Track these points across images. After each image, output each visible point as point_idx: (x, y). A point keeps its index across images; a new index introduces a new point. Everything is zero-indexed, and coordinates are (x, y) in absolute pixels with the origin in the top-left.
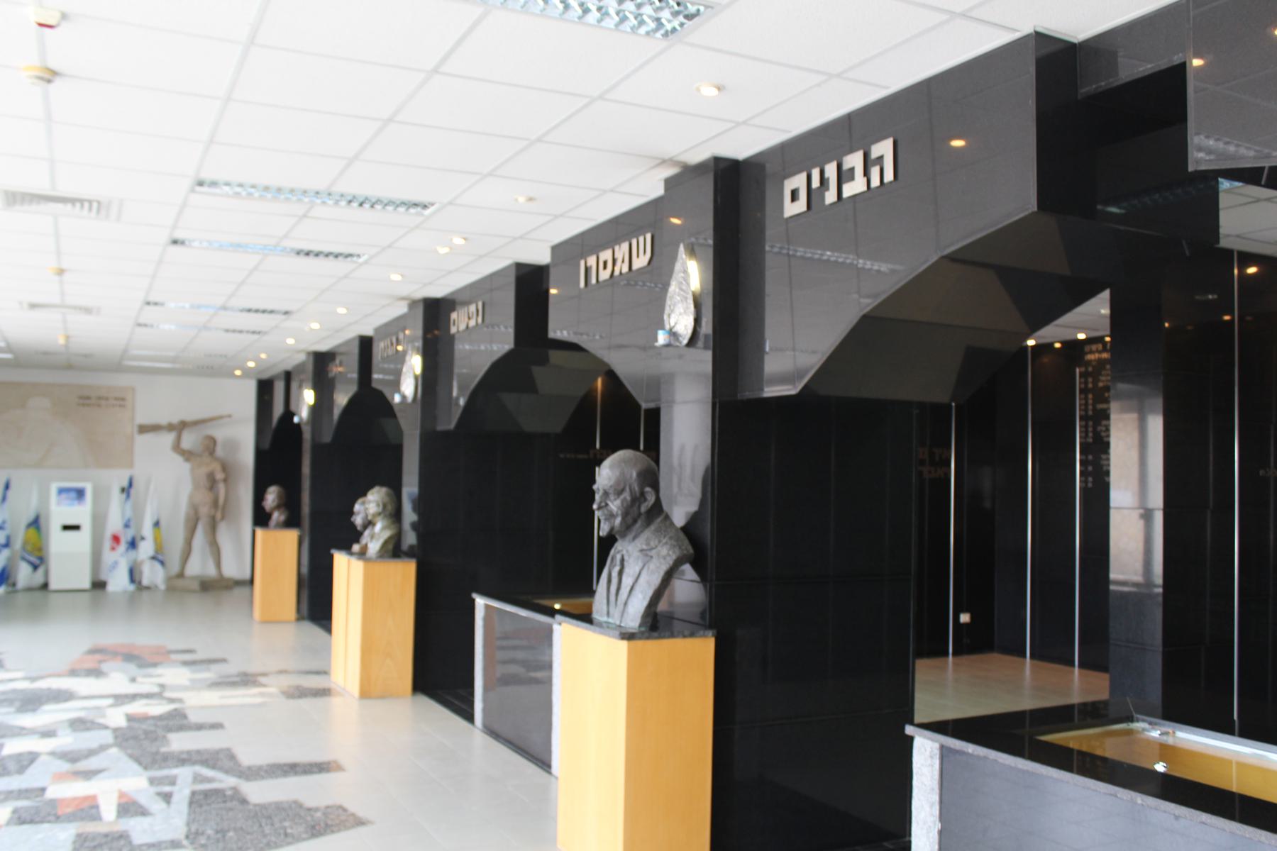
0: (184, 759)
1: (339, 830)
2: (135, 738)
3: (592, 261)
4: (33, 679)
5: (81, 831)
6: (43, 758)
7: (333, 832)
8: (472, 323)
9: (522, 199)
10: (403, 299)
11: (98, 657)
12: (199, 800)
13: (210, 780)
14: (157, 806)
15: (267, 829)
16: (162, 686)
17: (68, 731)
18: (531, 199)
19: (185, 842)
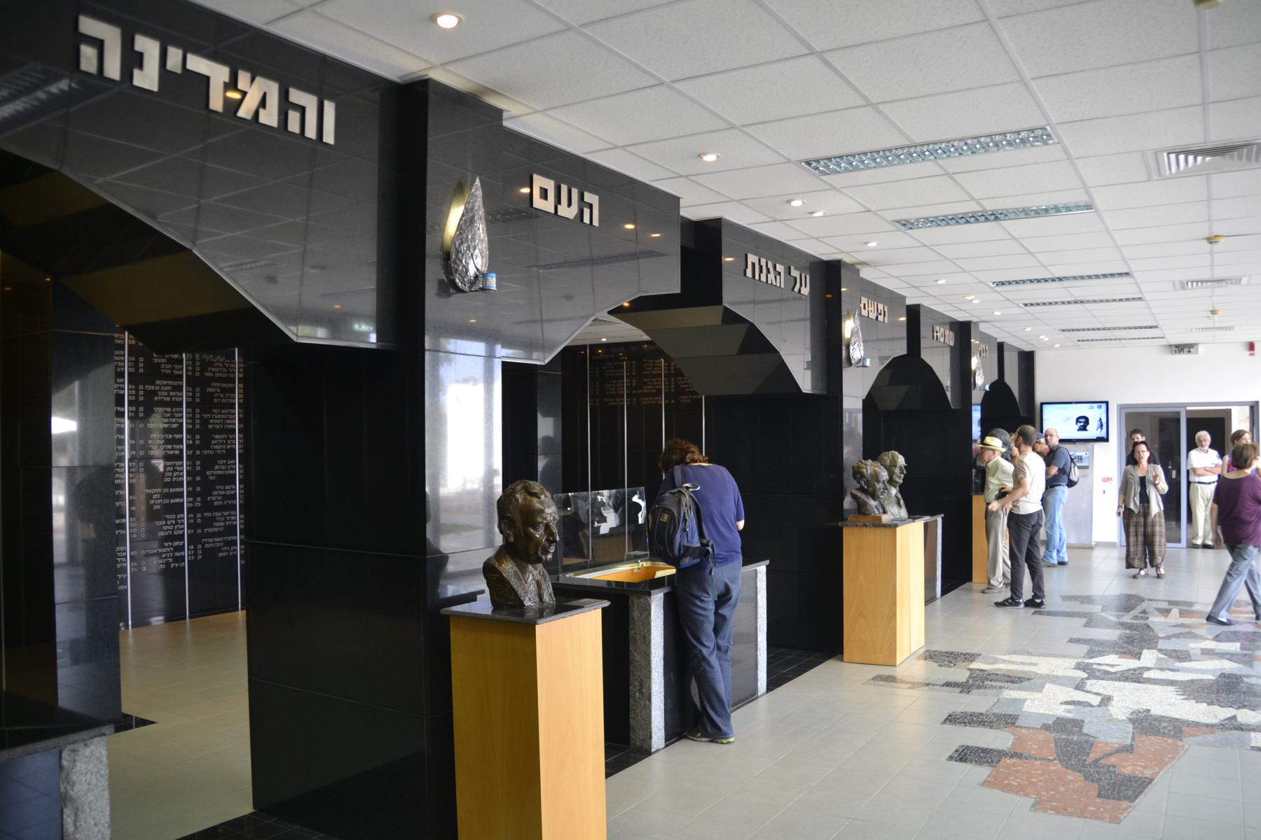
17: (1191, 652)
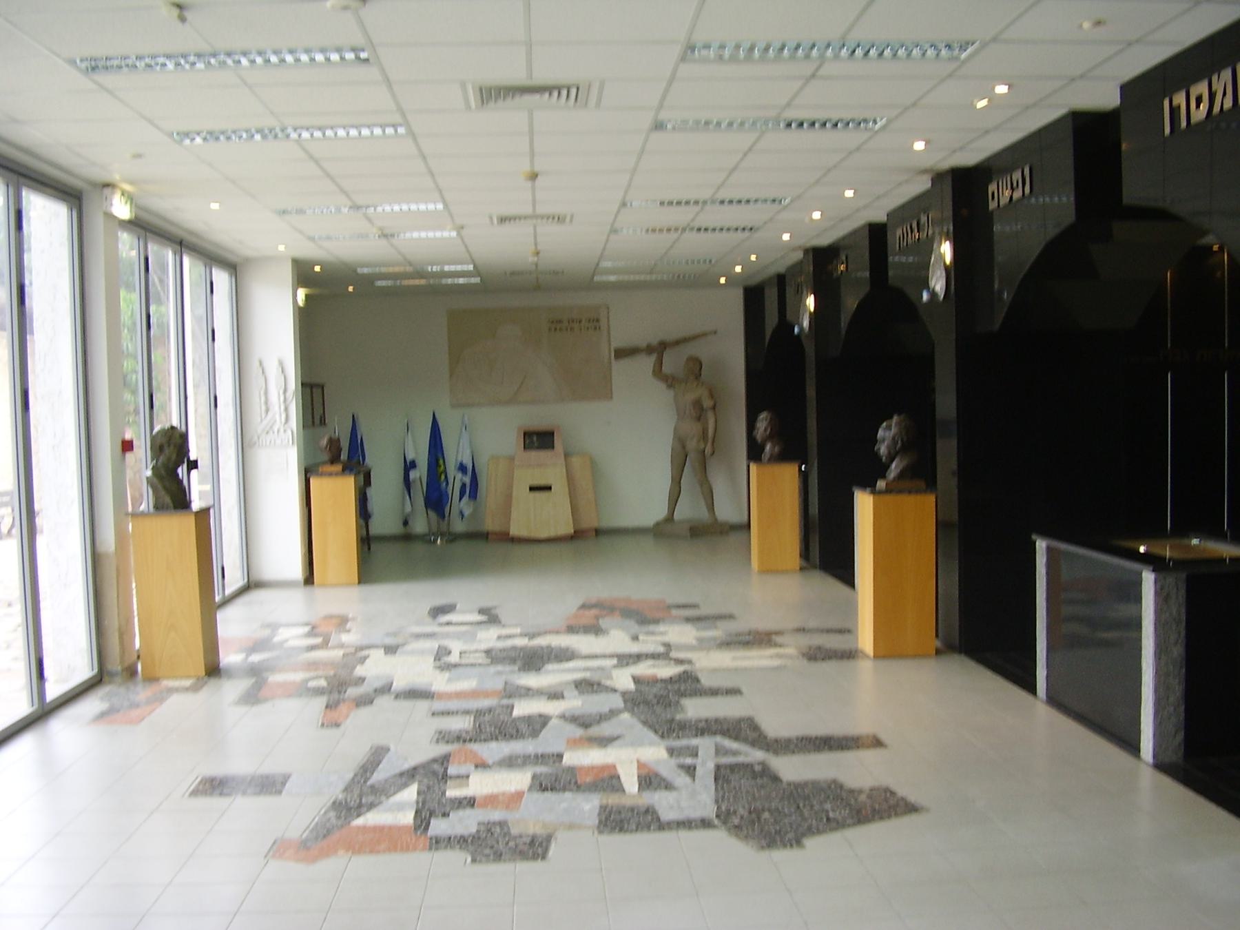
0: (706, 728)
1: (889, 817)
2: (647, 703)
3: (1180, 99)
4: (532, 636)
5: (604, 802)
6: (554, 722)
7: (881, 818)
8: (1017, 194)
9: (1086, 25)
10: (925, 171)
11: (594, 612)
12: (722, 775)
13: (735, 753)
14: (681, 780)
15: (806, 813)
16: (668, 646)
18: (1098, 23)
19: (716, 822)
